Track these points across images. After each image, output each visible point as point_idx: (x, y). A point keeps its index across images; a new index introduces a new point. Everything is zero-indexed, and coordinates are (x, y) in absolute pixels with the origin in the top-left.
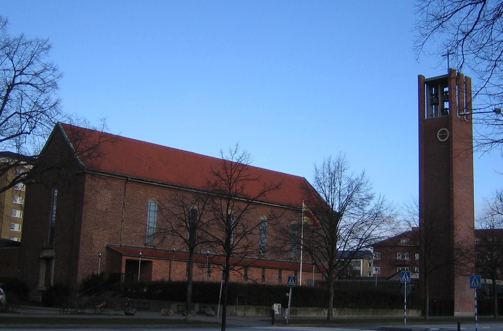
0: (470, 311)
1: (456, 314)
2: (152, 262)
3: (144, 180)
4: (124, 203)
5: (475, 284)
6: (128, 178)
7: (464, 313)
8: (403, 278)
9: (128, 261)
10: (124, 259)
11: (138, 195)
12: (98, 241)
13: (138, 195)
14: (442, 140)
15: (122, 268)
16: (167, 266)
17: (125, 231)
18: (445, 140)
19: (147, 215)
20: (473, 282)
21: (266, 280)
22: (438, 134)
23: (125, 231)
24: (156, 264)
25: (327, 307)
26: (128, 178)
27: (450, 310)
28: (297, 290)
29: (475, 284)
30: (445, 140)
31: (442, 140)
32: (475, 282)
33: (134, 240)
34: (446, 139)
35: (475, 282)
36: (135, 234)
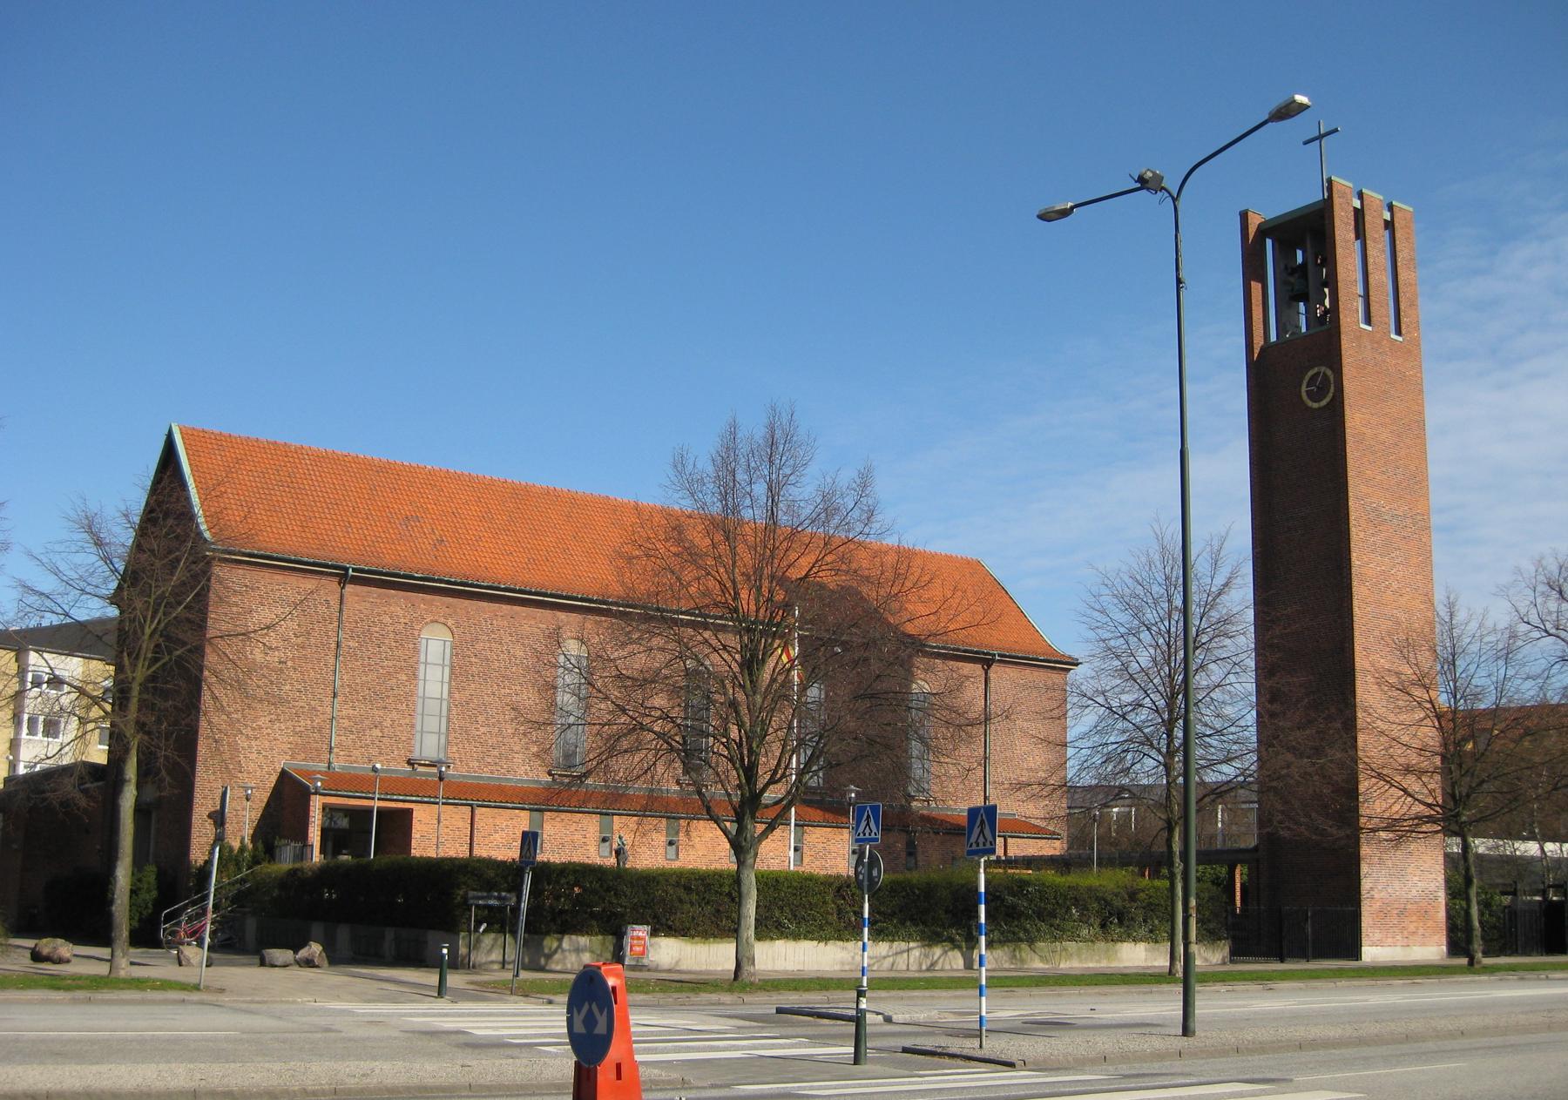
0: (1423, 944)
1: (1371, 953)
2: (410, 811)
3: (530, 593)
4: (338, 645)
5: (981, 840)
6: (346, 569)
7: (1398, 949)
8: (973, 840)
9: (325, 807)
10: (316, 803)
11: (387, 619)
12: (254, 756)
13: (387, 619)
14: (1315, 405)
15: (311, 829)
16: (461, 824)
17: (346, 723)
18: (1324, 403)
19: (415, 676)
20: (863, 824)
21: (806, 860)
22: (1304, 388)
23: (346, 723)
24: (423, 818)
25: (731, 930)
26: (346, 569)
27: (1351, 948)
28: (772, 885)
29: (981, 840)
30: (1324, 403)
31: (1315, 405)
32: (982, 831)
33: (375, 751)
34: (1328, 399)
35: (982, 831)
36: (377, 732)
